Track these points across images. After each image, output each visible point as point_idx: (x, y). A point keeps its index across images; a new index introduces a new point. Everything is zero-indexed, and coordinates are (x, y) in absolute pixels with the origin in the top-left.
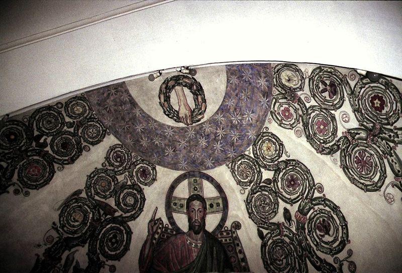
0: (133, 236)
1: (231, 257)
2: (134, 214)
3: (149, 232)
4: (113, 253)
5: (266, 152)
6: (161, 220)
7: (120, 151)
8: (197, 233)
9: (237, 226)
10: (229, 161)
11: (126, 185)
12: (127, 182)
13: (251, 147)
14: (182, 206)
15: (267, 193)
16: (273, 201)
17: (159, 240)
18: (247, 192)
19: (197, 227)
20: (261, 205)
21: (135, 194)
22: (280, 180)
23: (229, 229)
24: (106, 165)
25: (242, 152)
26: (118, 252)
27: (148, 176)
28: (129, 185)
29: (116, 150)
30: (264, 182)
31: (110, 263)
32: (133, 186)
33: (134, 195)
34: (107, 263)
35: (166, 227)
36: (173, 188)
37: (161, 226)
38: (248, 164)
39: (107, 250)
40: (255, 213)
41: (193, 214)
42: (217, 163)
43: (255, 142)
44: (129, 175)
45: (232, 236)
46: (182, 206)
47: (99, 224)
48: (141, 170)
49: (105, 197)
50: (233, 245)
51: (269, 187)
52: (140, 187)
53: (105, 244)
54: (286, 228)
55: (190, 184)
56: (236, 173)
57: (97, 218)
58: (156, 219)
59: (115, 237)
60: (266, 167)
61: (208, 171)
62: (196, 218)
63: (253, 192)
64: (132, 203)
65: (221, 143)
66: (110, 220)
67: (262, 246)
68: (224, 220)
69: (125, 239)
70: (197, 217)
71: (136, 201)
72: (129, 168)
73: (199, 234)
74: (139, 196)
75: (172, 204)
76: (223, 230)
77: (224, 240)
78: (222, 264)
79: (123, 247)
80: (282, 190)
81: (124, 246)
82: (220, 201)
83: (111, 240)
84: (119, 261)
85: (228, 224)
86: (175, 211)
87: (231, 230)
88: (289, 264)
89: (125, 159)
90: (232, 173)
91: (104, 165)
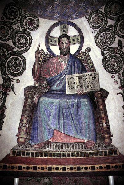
0: (27, 62)
1: (85, 66)
2: (26, 49)
3: (36, 58)
4: (17, 72)
5: (113, 10)
6: (43, 50)
7: (13, 8)
8: (65, 55)
9: (89, 50)
10: (87, 14)
11: (19, 32)
12: (20, 29)
13: (104, 6)
14: (55, 41)
15: (109, 33)
16: (112, 36)
17: (42, 62)
18: (96, 32)
19: (65, 52)
20: (104, 39)
21: (25, 36)
22: (118, 25)
23: (84, 52)
24: (4, 19)
25: (97, 9)
26: (19, 71)
27: (34, 25)
28: (21, 31)
29: (11, 7)
30: (108, 27)
31: (16, 78)
32: (24, 32)
33: (25, 37)
34: (14, 79)
35: (46, 54)
36: (49, 31)
37: (43, 54)
38: (100, 17)
39: (12, 72)
40: (100, 43)
41: (62, 46)
42: (79, 16)
43: (108, 3)
44: (21, 24)
45: (86, 56)
46: (55, 41)
47: (4, 57)
48: (29, 21)
49: (6, 40)
50: (86, 60)
51: (111, 29)
52: (28, 32)
53: (10, 69)
54: (118, 50)
55: (61, 28)
56: (91, 22)
57: (2, 54)
58: (39, 50)
59: (16, 63)
60: (111, 18)
61: (73, 20)
62: (65, 47)
63: (100, 32)
64: (24, 42)
65: (84, 3)
66: (11, 54)
67: (103, 59)
68: (81, 47)
69: (22, 64)
70: (65, 47)
71: (26, 41)
72: (21, 20)
73: (66, 56)
74: (28, 38)
75: (49, 41)
76: (80, 52)
77: (81, 58)
78: (80, 69)
79: (21, 69)
80: (119, 31)
81: (22, 68)
82: (79, 38)
83: (13, 66)
84: (21, 76)
85: (84, 49)
86: (51, 44)
87: (85, 53)
88: (119, 66)
89: (17, 14)
90: (88, 22)
91: (3, 18)
